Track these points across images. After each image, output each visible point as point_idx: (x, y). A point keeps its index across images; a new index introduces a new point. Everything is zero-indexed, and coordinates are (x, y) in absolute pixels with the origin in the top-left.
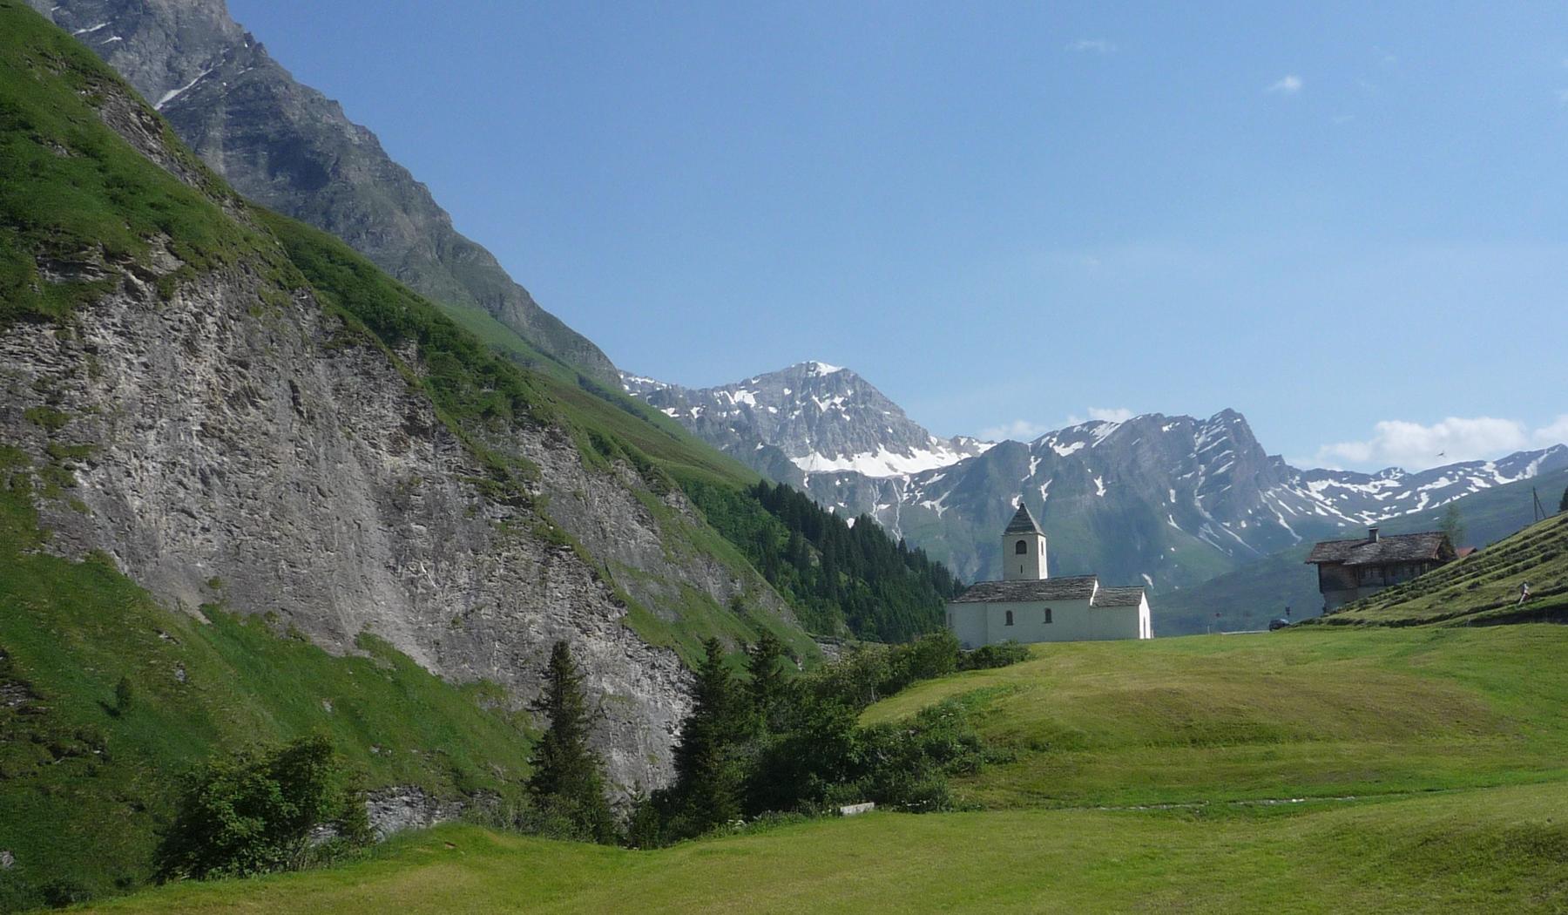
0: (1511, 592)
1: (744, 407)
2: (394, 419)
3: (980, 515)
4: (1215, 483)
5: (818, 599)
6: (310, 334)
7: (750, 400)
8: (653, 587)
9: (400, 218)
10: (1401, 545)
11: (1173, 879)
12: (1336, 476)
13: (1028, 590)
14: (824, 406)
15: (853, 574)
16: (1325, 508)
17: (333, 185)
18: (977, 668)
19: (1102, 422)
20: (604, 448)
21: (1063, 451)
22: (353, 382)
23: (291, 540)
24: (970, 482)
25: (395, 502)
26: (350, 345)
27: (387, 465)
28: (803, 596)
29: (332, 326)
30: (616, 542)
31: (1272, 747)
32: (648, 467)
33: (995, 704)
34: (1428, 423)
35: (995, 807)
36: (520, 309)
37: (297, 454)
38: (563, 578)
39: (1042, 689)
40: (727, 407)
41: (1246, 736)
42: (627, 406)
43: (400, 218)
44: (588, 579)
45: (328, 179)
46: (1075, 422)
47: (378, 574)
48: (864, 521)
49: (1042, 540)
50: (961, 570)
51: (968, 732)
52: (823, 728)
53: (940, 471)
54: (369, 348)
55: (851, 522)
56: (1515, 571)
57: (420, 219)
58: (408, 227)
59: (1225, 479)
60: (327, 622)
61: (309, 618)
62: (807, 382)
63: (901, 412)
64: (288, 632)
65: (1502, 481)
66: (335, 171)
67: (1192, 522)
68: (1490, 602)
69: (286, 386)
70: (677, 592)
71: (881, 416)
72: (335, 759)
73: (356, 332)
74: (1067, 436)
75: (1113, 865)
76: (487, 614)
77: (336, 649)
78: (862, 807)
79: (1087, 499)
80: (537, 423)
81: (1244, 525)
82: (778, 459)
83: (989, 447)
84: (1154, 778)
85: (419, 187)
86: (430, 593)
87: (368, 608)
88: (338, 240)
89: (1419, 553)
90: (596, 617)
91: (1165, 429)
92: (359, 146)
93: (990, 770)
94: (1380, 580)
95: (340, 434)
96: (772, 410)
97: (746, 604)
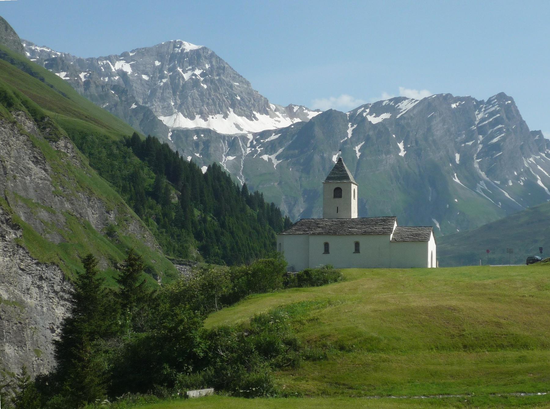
4: (490, 149)
5: (175, 230)
7: (128, 69)
8: (44, 214)
13: (341, 227)
14: (186, 76)
19: (405, 99)
24: (300, 140)
28: (164, 226)
30: (15, 178)
31: (524, 353)
32: (43, 118)
33: (312, 314)
35: (309, 394)
40: (110, 74)
41: (505, 343)
42: (27, 68)
46: (386, 97)
48: (215, 169)
49: (354, 187)
50: (290, 212)
51: (290, 335)
53: (277, 131)
55: (204, 169)
59: (497, 147)
62: (173, 57)
63: (248, 83)
70: (62, 219)
71: (231, 87)
74: (377, 108)
78: (204, 392)
79: (391, 159)
82: (148, 117)
83: (316, 114)
84: (433, 374)
91: (454, 106)
93: (307, 365)
96: (145, 77)
97: (118, 231)
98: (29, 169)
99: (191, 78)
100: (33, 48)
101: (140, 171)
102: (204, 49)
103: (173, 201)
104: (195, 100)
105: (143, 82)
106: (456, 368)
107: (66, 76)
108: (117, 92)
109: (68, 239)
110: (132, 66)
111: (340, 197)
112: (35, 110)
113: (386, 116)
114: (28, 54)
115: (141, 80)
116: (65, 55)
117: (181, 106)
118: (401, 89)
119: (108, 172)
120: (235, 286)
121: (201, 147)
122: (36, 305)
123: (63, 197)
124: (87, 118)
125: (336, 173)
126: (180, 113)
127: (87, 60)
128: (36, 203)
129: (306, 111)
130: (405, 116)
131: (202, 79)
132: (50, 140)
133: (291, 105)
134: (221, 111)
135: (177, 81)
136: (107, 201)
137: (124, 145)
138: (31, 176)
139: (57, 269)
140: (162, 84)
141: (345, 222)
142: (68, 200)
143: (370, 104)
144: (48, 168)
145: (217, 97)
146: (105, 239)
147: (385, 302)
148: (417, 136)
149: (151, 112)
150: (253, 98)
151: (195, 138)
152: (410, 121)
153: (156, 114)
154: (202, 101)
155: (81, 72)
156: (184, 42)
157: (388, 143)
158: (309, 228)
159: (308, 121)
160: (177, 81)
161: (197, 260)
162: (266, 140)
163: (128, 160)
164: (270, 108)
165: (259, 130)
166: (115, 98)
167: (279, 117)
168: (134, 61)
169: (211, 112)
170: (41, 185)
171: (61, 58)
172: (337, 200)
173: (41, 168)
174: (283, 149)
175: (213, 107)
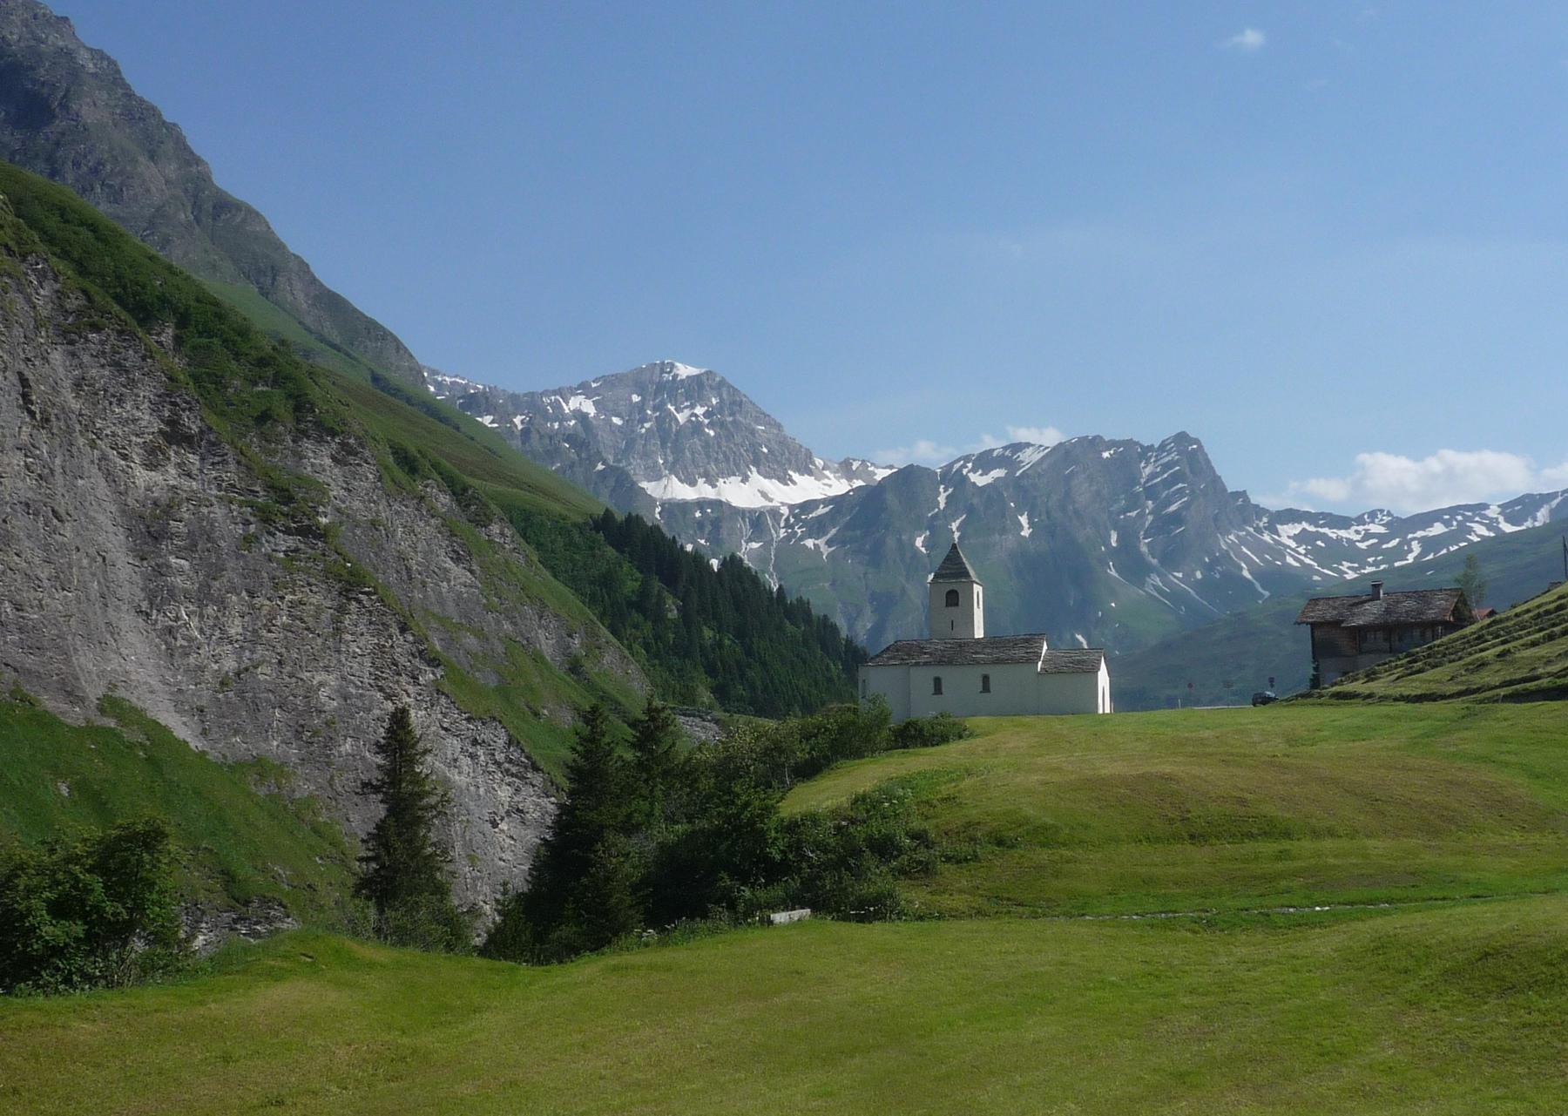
0: (1549, 662)
1: (580, 416)
2: (150, 423)
3: (875, 557)
4: (1166, 523)
5: (675, 660)
6: (44, 313)
7: (589, 408)
8: (471, 641)
9: (144, 166)
10: (1409, 604)
11: (1186, 1001)
12: (1311, 518)
13: (960, 652)
14: (681, 418)
16: (1297, 558)
17: (60, 124)
18: (905, 746)
19: (1028, 445)
20: (408, 463)
21: (979, 480)
22: (100, 374)
23: (18, 577)
24: (867, 516)
25: (150, 528)
26: (96, 328)
27: (140, 482)
28: (657, 656)
29: (73, 303)
30: (424, 584)
31: (1286, 845)
32: (465, 490)
33: (945, 790)
34: (1417, 458)
35: (956, 915)
36: (298, 285)
37: (27, 467)
38: (362, 628)
39: (1001, 772)
40: (560, 416)
41: (1255, 831)
42: (432, 410)
43: (144, 166)
44: (395, 630)
45: (54, 117)
47: (127, 621)
48: (732, 564)
50: (850, 628)
51: (916, 824)
52: (737, 816)
54: (120, 333)
55: (715, 563)
56: (1551, 637)
57: (171, 169)
58: (155, 180)
59: (1177, 519)
60: (63, 682)
61: (39, 677)
62: (661, 387)
63: (779, 426)
64: (12, 693)
65: (1508, 528)
66: (64, 106)
67: (1135, 569)
68: (1524, 673)
69: (14, 379)
70: (500, 649)
71: (753, 432)
72: (172, 848)
73: (104, 312)
74: (985, 461)
75: (1113, 984)
76: (265, 674)
77: (75, 716)
78: (797, 914)
80: (325, 431)
81: (1199, 575)
82: (623, 484)
83: (888, 472)
84: (1149, 881)
85: (172, 128)
86: (192, 646)
87: (114, 664)
88: (66, 188)
89: (1431, 614)
90: (404, 679)
91: (1106, 455)
92: (95, 75)
93: (948, 870)
94: (1386, 646)
95: (81, 441)
96: (616, 421)
97: (587, 665)
98: (446, 570)
99: (689, 421)
103: (670, 615)
106: (1181, 870)
113: (998, 473)
114: (432, 389)
117: (674, 463)
118: (1010, 429)
120: (812, 749)
121: (708, 528)
122: (468, 784)
124: (532, 488)
138: (449, 581)
147: (1058, 769)
149: (628, 475)
151: (698, 514)
154: (708, 457)
157: (1003, 516)
161: (711, 707)
171: (484, 393)
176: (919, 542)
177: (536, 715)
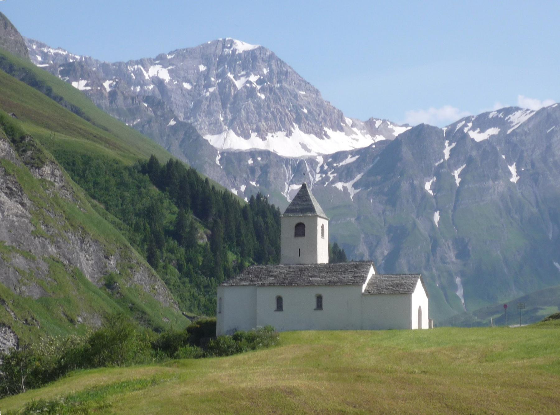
1: (159, 82)
3: (392, 198)
5: (204, 280)
7: (164, 75)
14: (239, 84)
15: (242, 254)
19: (517, 109)
28: (188, 275)
32: (23, 138)
40: (142, 82)
42: (33, 80)
46: (494, 108)
49: (322, 223)
53: (353, 153)
62: (222, 60)
63: (317, 92)
70: (44, 267)
71: (296, 96)
74: (482, 122)
79: (500, 186)
82: (191, 139)
83: (403, 130)
99: (245, 86)
100: (46, 51)
101: (159, 204)
102: (261, 49)
103: (200, 242)
104: (250, 114)
105: (184, 92)
107: (87, 85)
108: (151, 104)
109: (50, 292)
110: (170, 72)
111: (303, 235)
112: (12, 127)
113: (493, 131)
114: (39, 58)
115: (182, 90)
116: (86, 58)
117: (232, 121)
119: (117, 206)
121: (258, 173)
123: (46, 239)
124: (95, 138)
125: (298, 204)
126: (231, 131)
127: (114, 64)
128: (9, 246)
129: (391, 127)
130: (518, 131)
131: (259, 87)
132: (32, 166)
133: (372, 118)
134: (284, 127)
135: (227, 90)
136: (107, 244)
137: (139, 172)
139: (8, 331)
140: (208, 94)
141: (307, 268)
142: (53, 242)
143: (473, 117)
144: (25, 201)
145: (278, 109)
146: (101, 292)
148: (534, 156)
149: (194, 130)
150: (324, 110)
151: (250, 162)
152: (524, 138)
153: (200, 132)
154: (259, 114)
155: (105, 80)
156: (236, 41)
158: (257, 277)
159: (393, 139)
160: (227, 90)
162: (341, 164)
163: (143, 190)
164: (345, 123)
165: (332, 150)
166: (149, 113)
167: (357, 134)
168: (173, 65)
169: (271, 129)
170: (16, 224)
171: (80, 63)
172: (300, 239)
173: (17, 201)
174: (362, 174)
175: (273, 123)
176: (427, 186)
177: (72, 321)
